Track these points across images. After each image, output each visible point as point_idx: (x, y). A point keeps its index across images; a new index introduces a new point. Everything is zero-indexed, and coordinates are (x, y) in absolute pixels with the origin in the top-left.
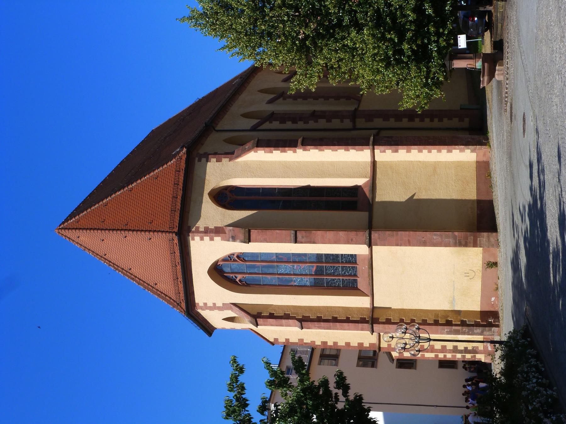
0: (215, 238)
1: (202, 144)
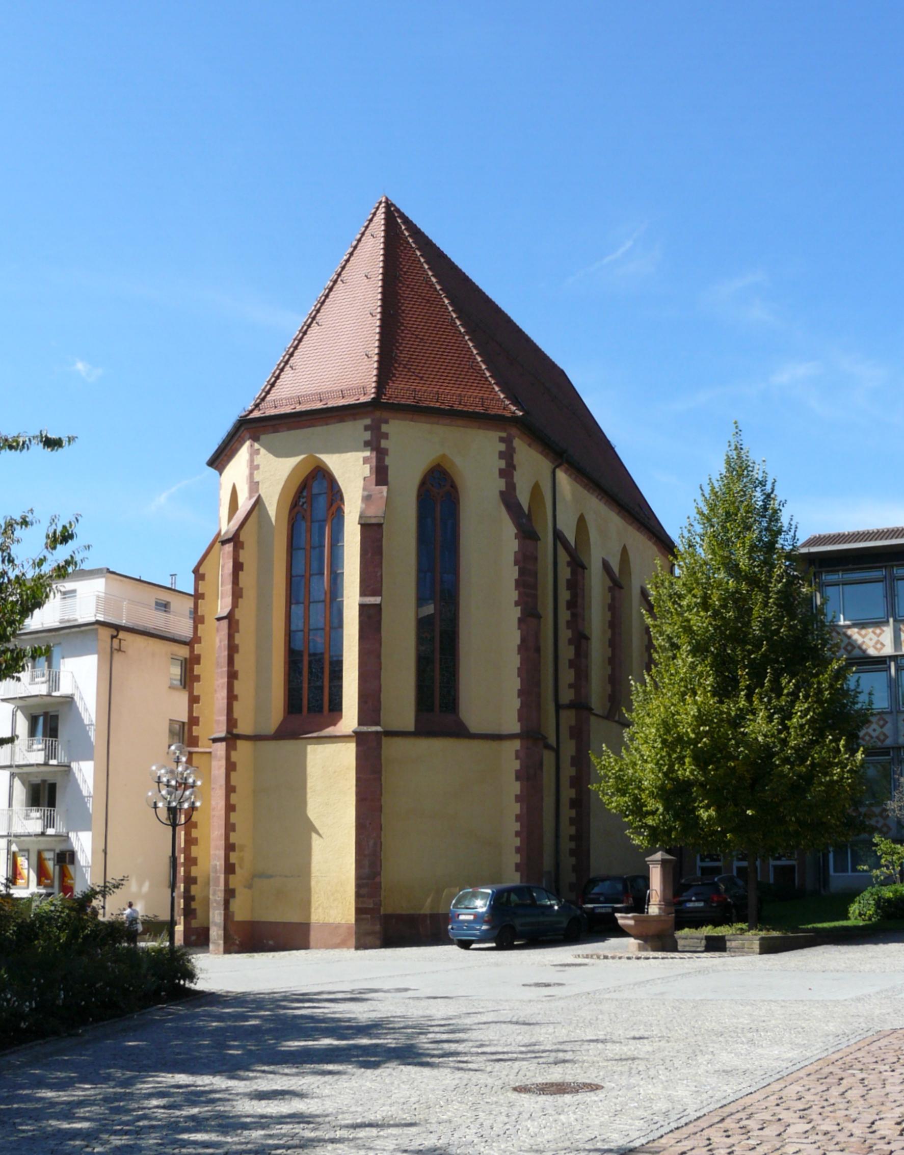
0: (368, 466)
1: (530, 445)
